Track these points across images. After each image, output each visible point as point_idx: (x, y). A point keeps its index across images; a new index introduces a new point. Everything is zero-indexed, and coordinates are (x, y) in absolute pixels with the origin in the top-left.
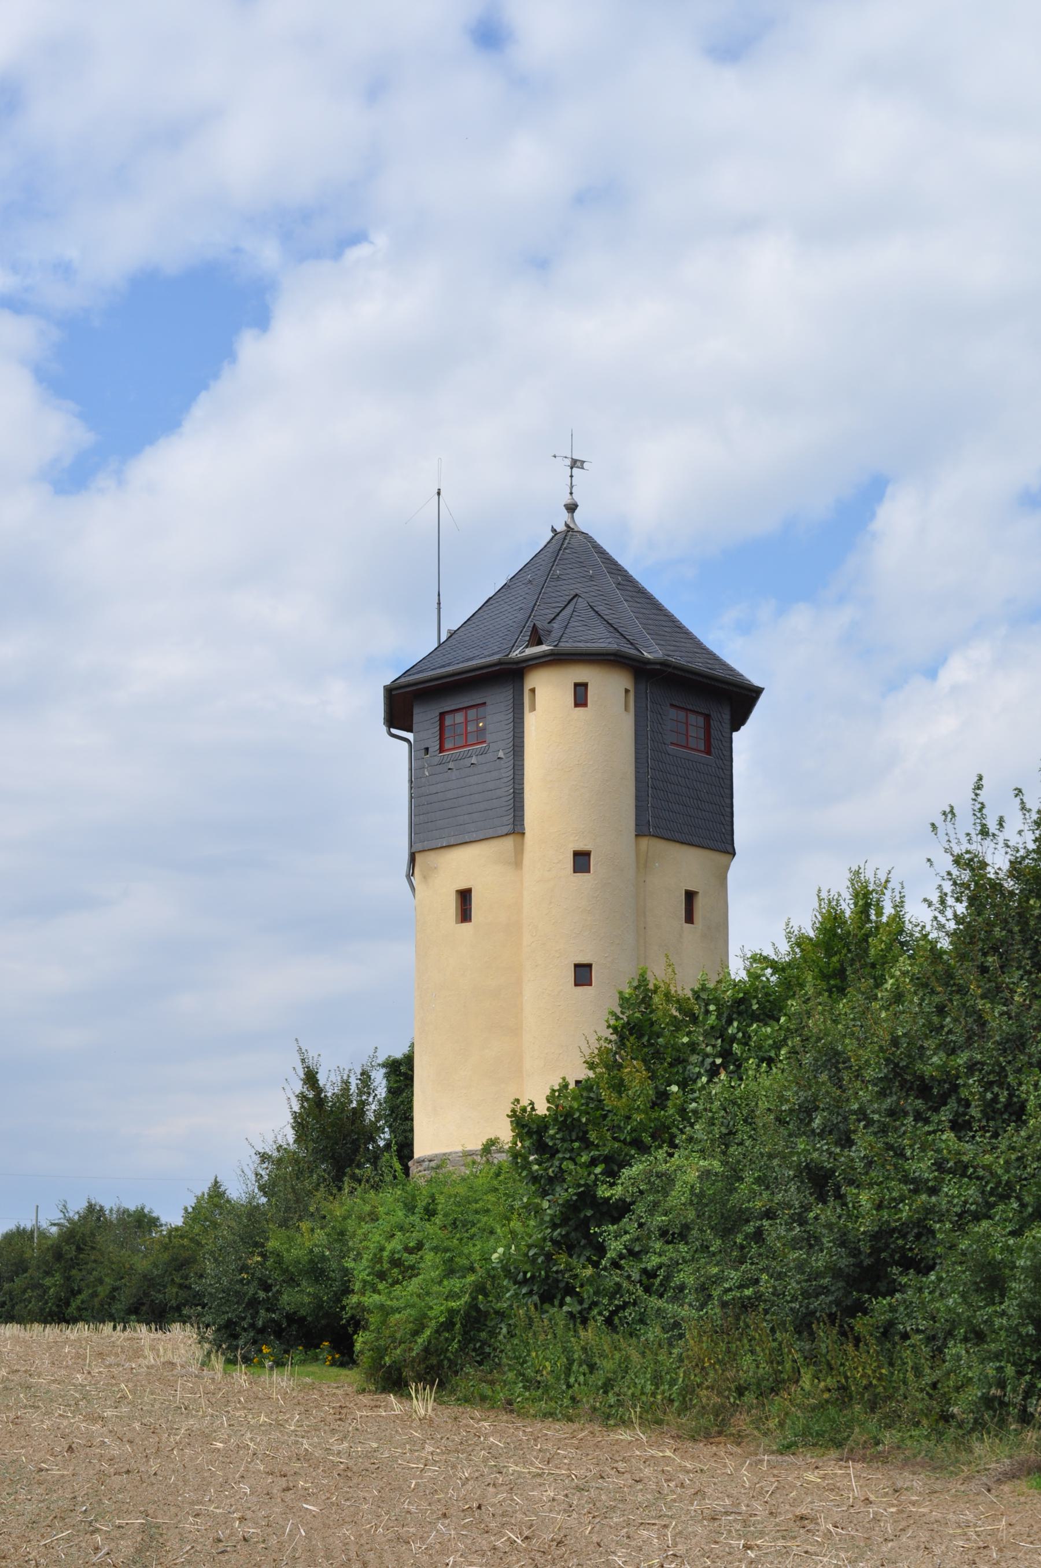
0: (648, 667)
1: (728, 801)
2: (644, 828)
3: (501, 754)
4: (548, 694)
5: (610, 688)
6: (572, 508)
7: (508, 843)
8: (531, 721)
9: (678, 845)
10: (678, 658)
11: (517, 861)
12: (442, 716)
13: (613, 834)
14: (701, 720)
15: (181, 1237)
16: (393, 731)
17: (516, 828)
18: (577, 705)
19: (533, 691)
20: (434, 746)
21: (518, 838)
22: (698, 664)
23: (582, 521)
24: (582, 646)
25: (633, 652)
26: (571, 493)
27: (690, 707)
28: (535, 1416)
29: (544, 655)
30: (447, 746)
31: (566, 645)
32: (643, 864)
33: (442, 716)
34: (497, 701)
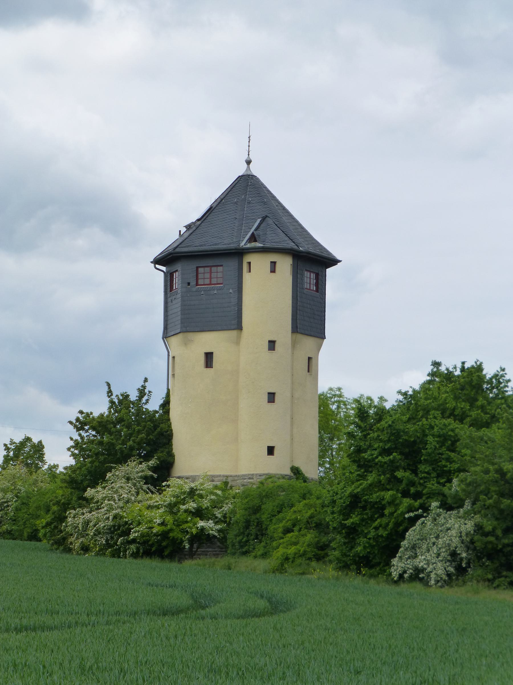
0: (301, 254)
1: (323, 314)
2: (295, 329)
3: (231, 291)
4: (258, 265)
5: (285, 264)
6: (249, 162)
7: (234, 333)
8: (247, 277)
9: (306, 336)
10: (312, 250)
11: (237, 342)
12: (197, 268)
13: (283, 332)
14: (313, 276)
15: (199, 513)
16: (157, 266)
17: (239, 327)
18: (271, 272)
19: (249, 263)
20: (193, 283)
21: (239, 331)
22: (317, 252)
23: (255, 170)
24: (275, 245)
25: (296, 247)
26: (249, 155)
27: (312, 270)
28: (364, 575)
29: (259, 248)
30: (200, 282)
31: (268, 245)
32: (294, 344)
33: (197, 268)
34: (231, 264)
